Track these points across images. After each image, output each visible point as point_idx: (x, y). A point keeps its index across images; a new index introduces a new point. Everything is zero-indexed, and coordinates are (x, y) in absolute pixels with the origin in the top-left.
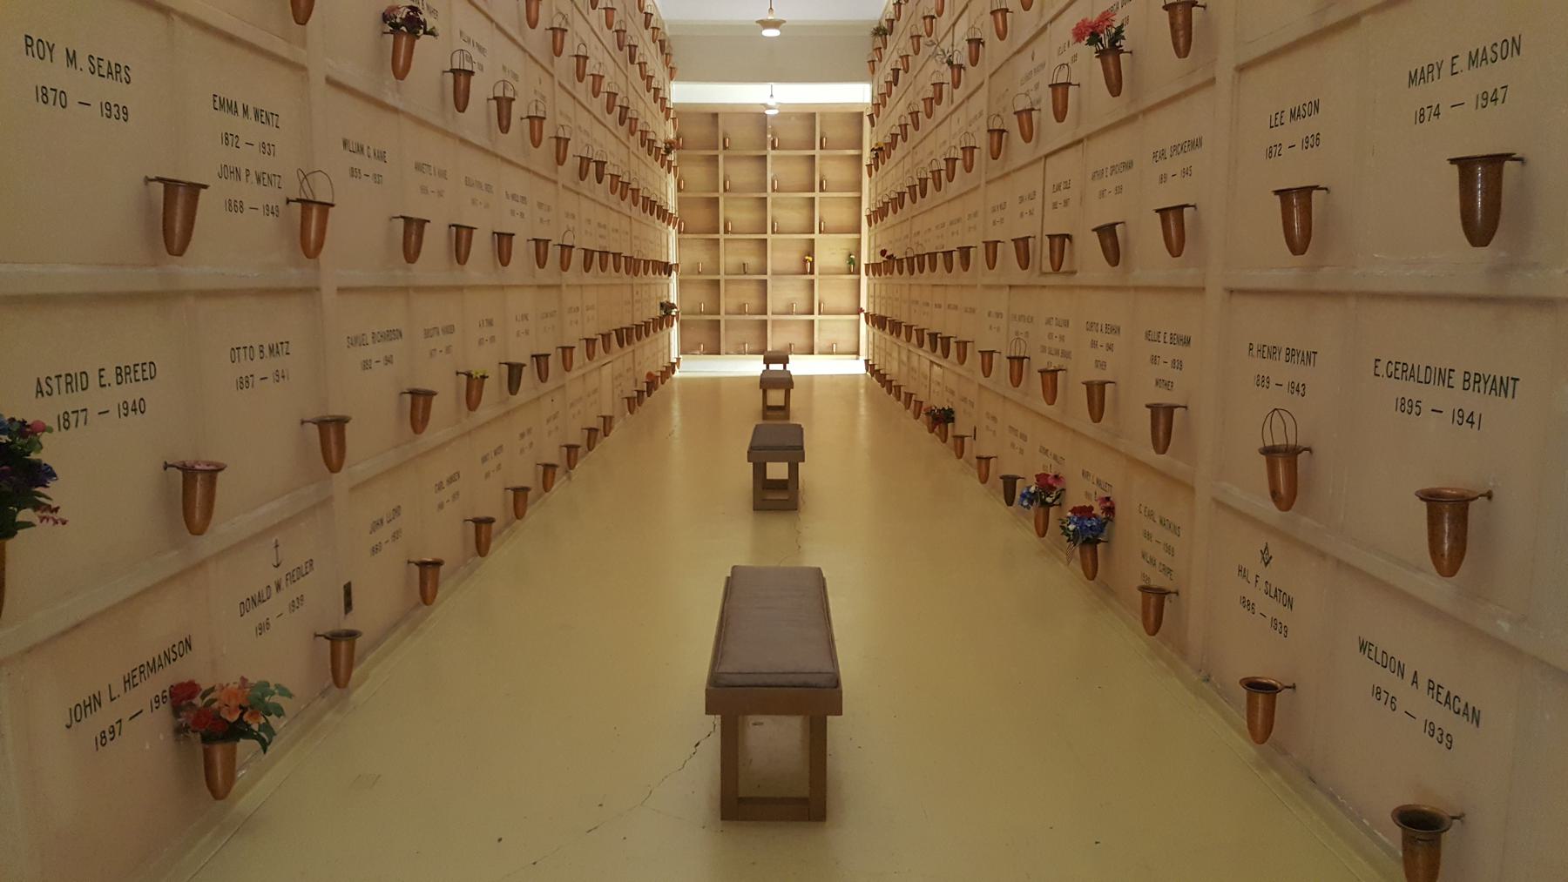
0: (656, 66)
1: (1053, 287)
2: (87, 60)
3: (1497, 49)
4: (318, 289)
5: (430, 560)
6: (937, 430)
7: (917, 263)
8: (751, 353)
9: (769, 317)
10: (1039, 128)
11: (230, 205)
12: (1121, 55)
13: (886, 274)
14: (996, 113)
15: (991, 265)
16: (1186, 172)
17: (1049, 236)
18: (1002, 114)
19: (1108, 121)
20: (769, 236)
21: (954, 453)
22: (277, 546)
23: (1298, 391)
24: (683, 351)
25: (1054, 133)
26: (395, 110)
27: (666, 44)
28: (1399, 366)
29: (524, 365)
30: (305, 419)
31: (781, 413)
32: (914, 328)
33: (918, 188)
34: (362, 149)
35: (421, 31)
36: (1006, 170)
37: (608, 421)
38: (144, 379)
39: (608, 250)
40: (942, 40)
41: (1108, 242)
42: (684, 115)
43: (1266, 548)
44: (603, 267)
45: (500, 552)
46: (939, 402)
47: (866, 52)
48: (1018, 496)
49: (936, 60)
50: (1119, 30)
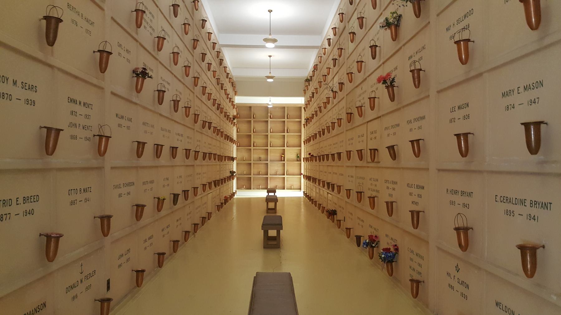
0: (230, 90)
1: (372, 167)
2: (21, 84)
3: (534, 85)
4: (103, 168)
5: (140, 270)
6: (330, 218)
7: (322, 158)
8: (262, 189)
9: (269, 176)
10: (364, 113)
11: (72, 137)
12: (394, 88)
13: (310, 161)
14: (349, 107)
15: (349, 159)
16: (420, 128)
17: (370, 149)
18: (351, 108)
19: (391, 110)
20: (269, 148)
21: (337, 226)
22: (82, 265)
23: (466, 207)
24: (238, 188)
25: (370, 114)
26: (136, 104)
27: (234, 83)
28: (505, 198)
29: (180, 194)
30: (96, 216)
31: (274, 211)
32: (321, 180)
33: (321, 132)
34: (123, 117)
35: (147, 77)
36: (353, 127)
37: (210, 214)
38: (34, 202)
39: (212, 153)
40: (329, 83)
41: (392, 152)
42: (240, 107)
43: (457, 265)
44: (210, 159)
45: (168, 266)
46: (331, 207)
47: (302, 87)
48: (362, 244)
49: (328, 90)
50: (393, 79)
